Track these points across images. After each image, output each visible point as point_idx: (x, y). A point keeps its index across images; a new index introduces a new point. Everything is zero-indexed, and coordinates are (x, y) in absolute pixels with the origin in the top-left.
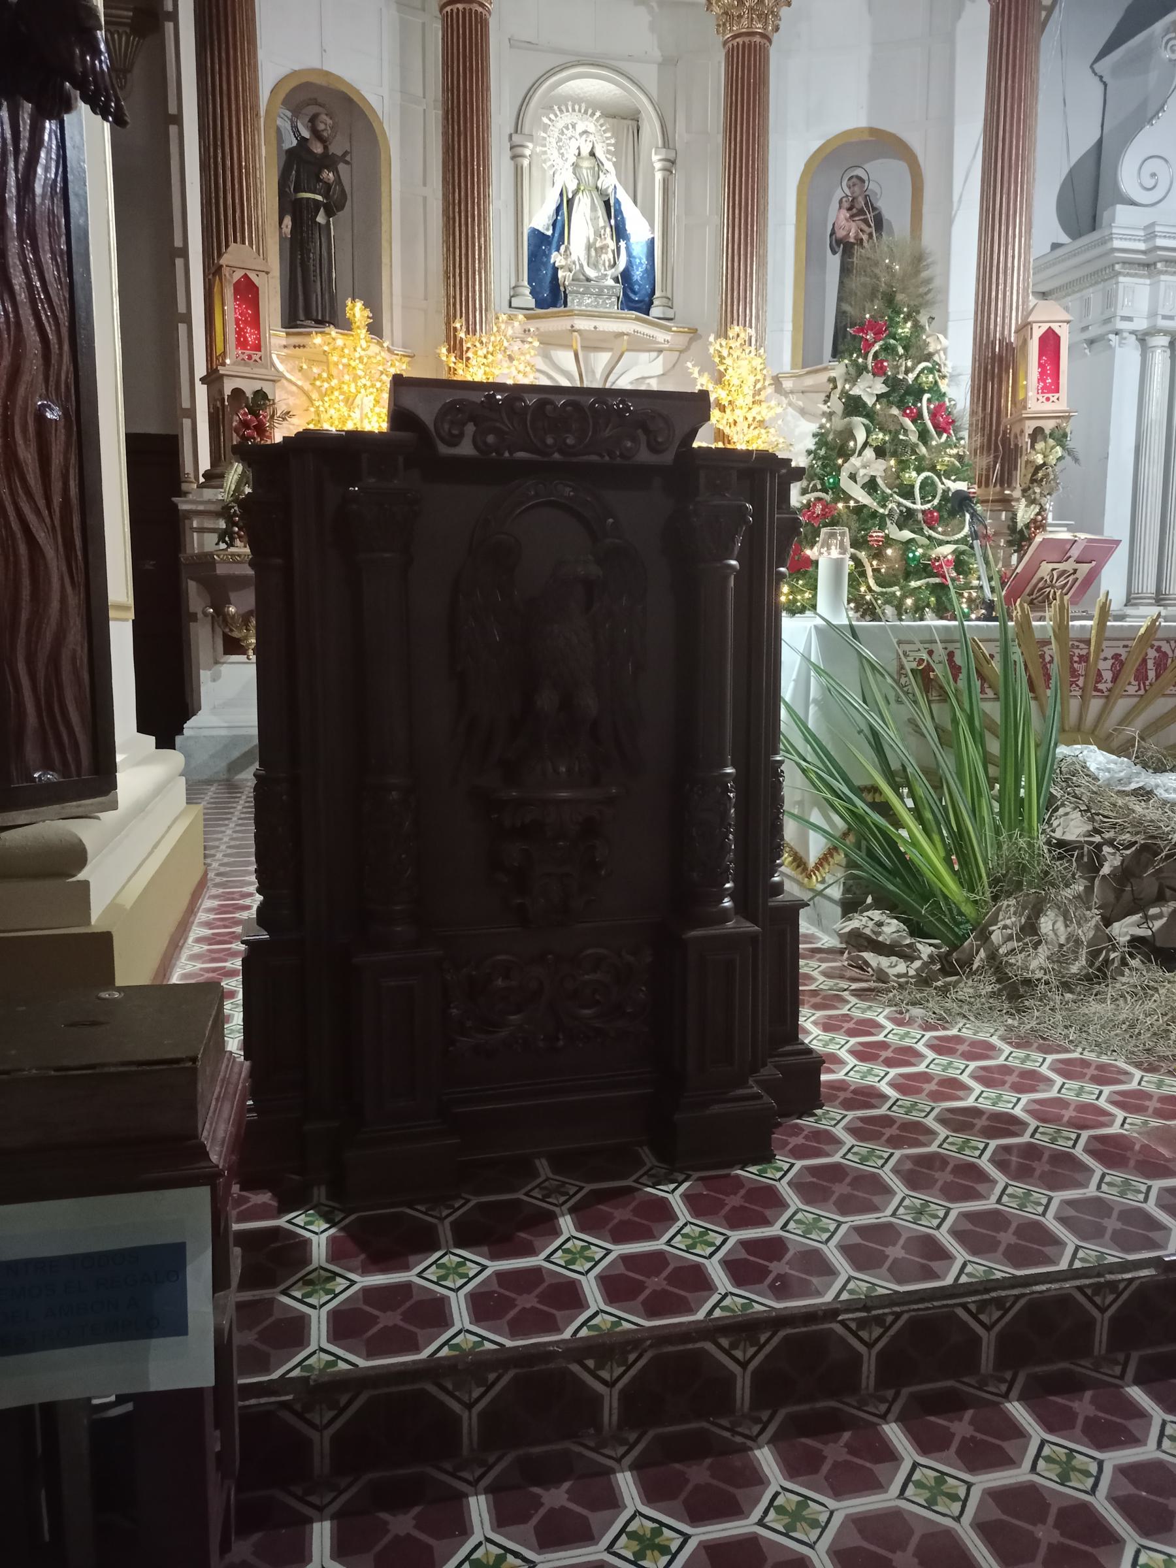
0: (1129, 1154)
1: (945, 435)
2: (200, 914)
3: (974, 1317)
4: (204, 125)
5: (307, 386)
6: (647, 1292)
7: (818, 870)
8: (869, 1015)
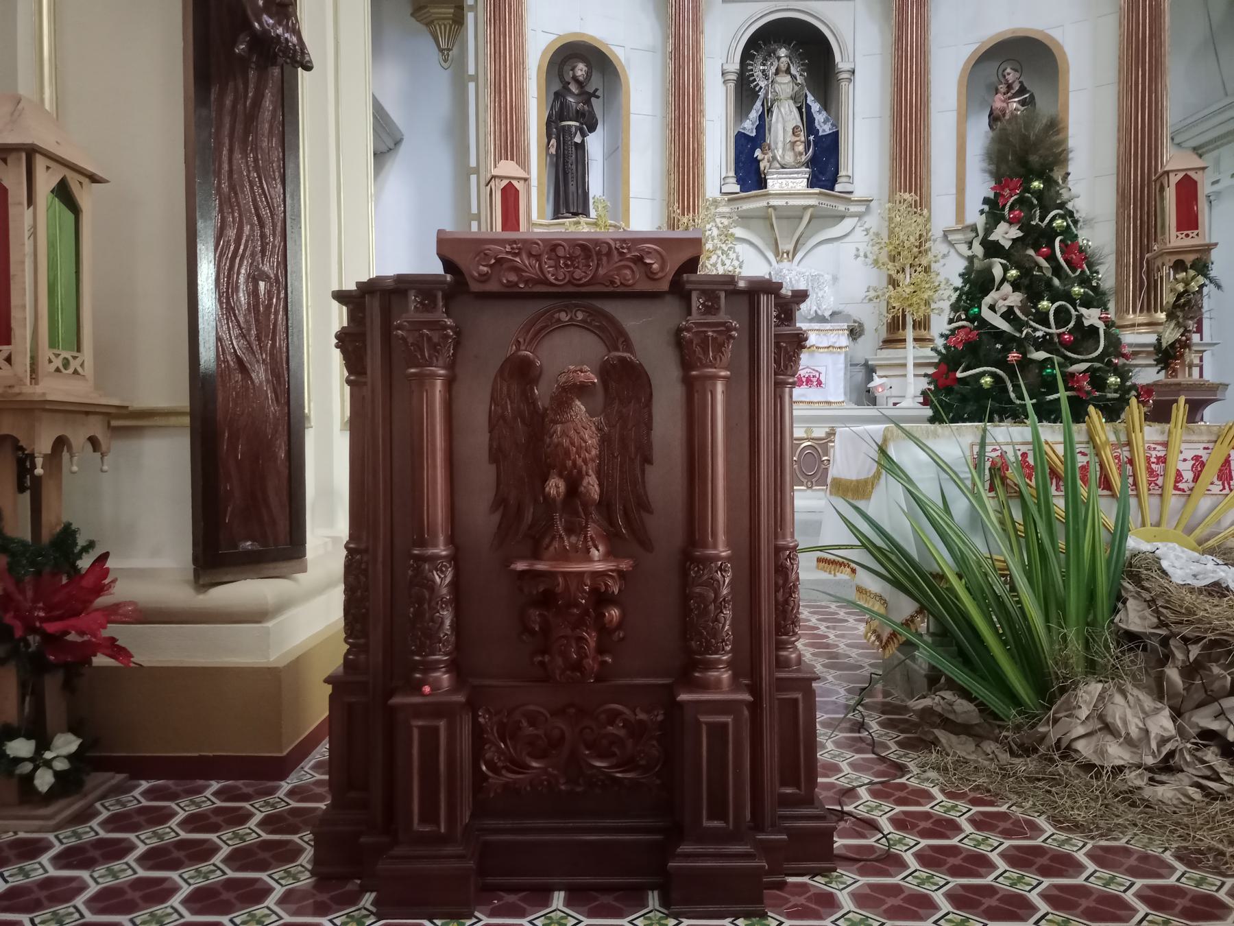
1: (1079, 271)
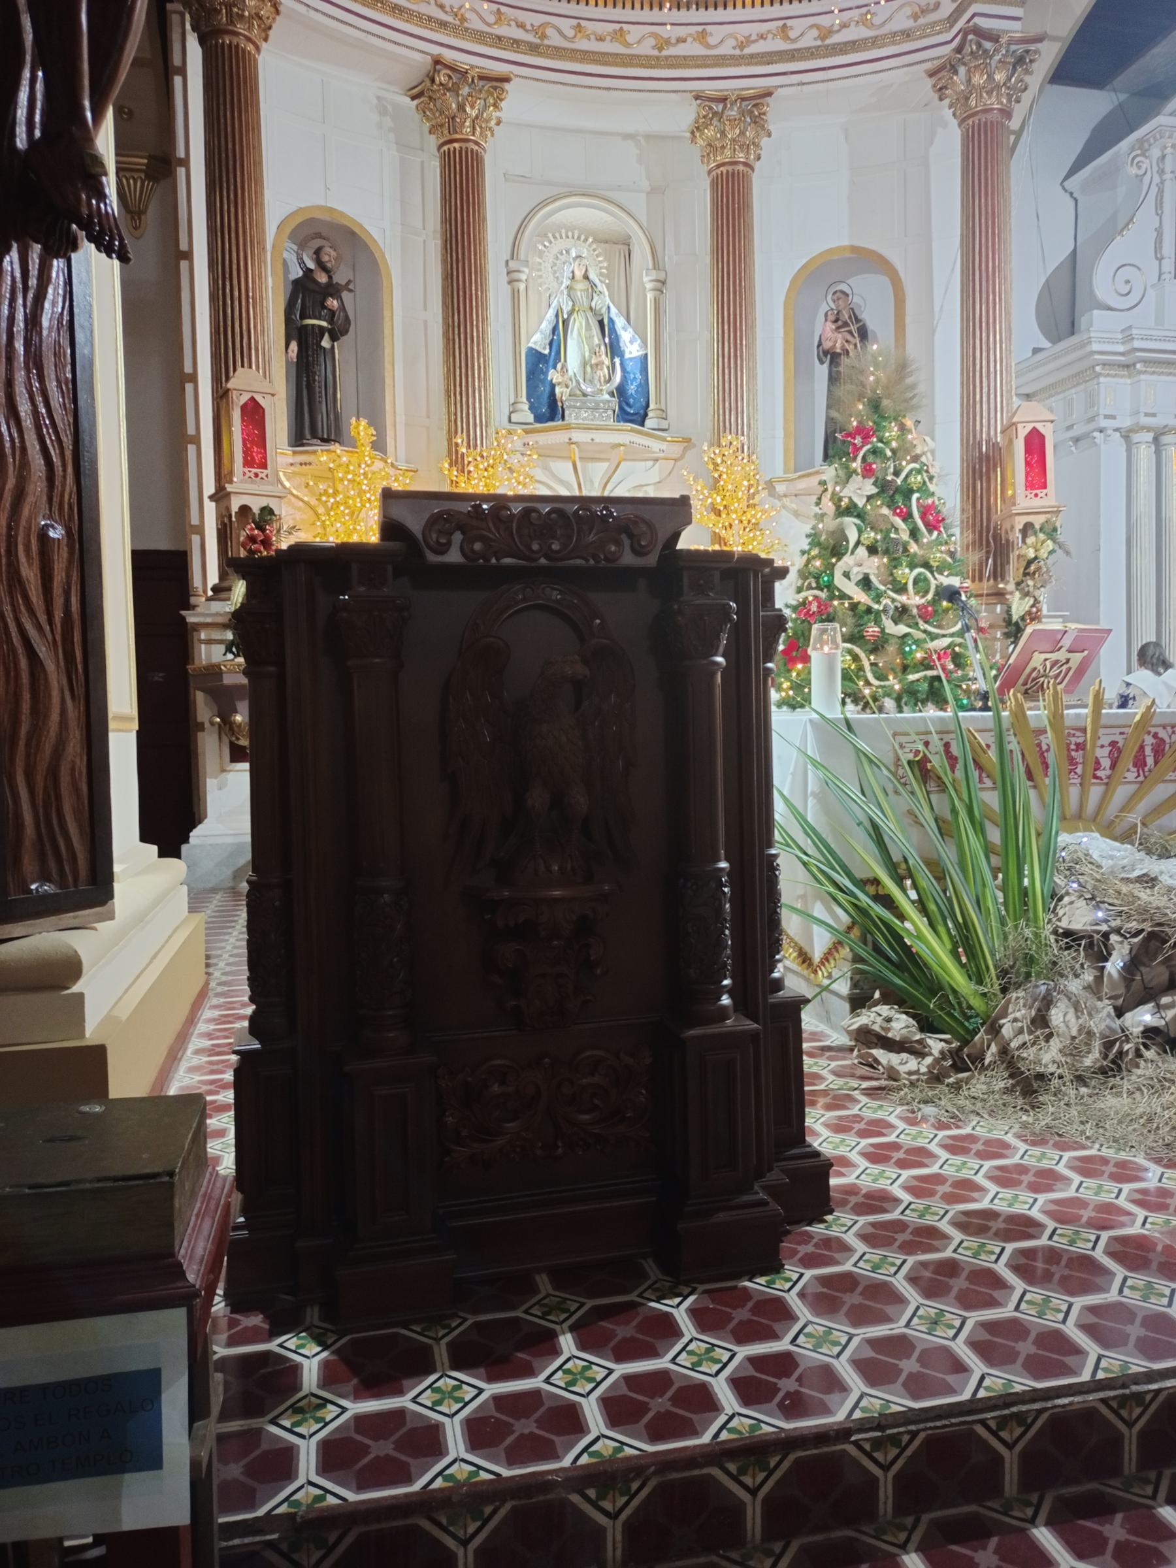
0: (1151, 1255)
1: (935, 533)
2: (200, 1024)
3: (995, 1434)
4: (213, 260)
5: (313, 502)
6: (650, 1415)
7: (824, 965)
8: (880, 1115)
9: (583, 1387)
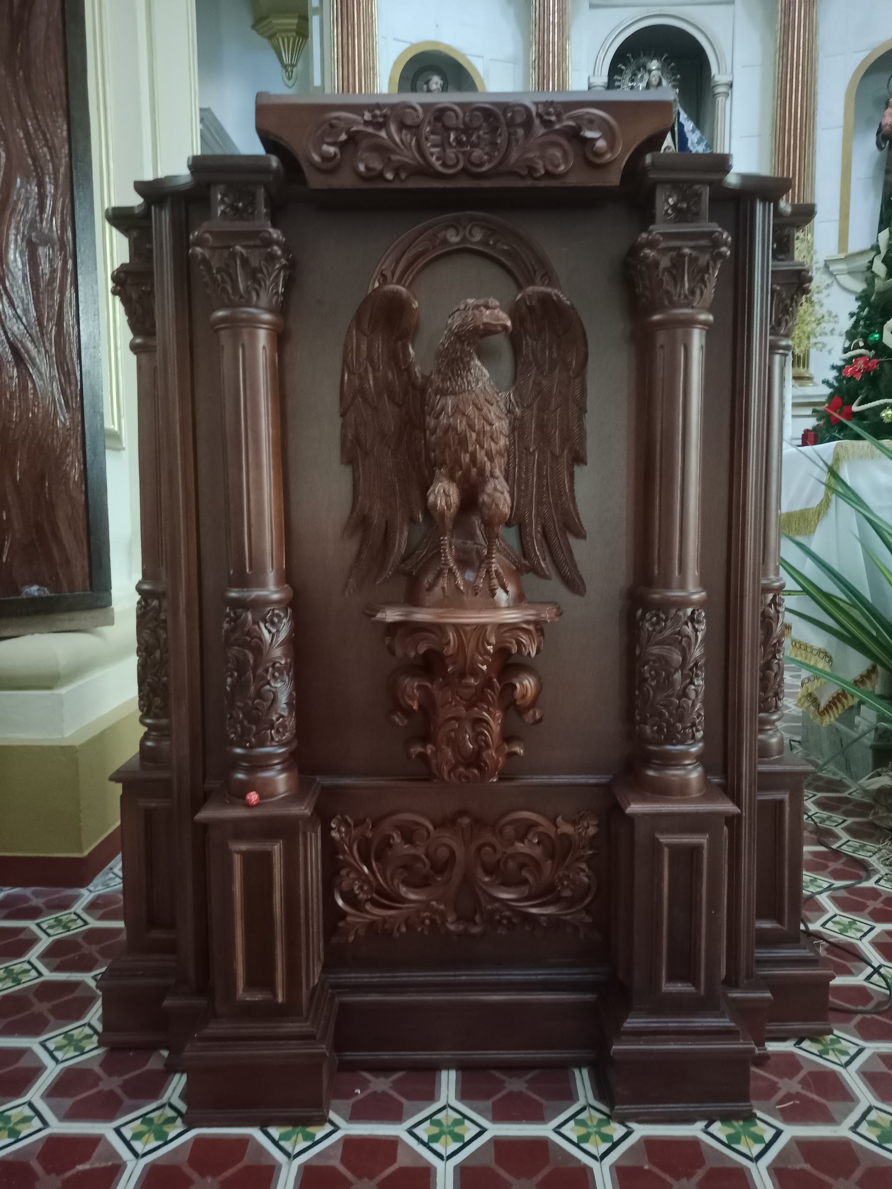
9: (446, 1146)
